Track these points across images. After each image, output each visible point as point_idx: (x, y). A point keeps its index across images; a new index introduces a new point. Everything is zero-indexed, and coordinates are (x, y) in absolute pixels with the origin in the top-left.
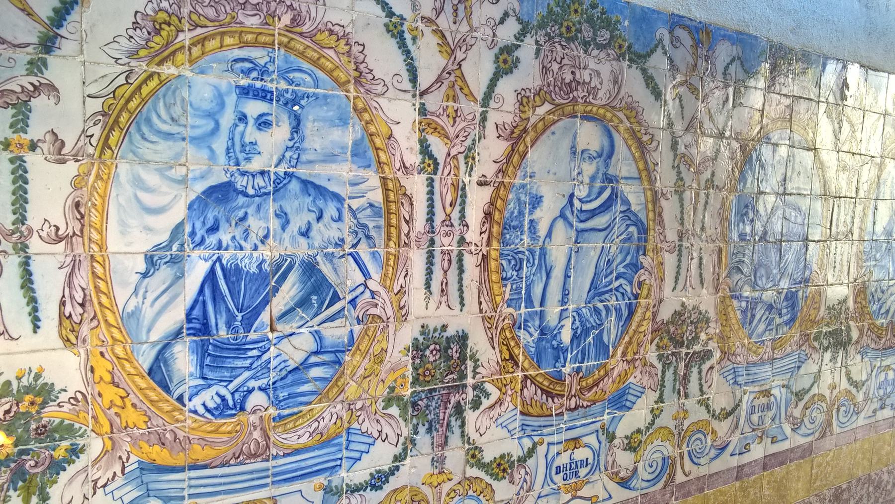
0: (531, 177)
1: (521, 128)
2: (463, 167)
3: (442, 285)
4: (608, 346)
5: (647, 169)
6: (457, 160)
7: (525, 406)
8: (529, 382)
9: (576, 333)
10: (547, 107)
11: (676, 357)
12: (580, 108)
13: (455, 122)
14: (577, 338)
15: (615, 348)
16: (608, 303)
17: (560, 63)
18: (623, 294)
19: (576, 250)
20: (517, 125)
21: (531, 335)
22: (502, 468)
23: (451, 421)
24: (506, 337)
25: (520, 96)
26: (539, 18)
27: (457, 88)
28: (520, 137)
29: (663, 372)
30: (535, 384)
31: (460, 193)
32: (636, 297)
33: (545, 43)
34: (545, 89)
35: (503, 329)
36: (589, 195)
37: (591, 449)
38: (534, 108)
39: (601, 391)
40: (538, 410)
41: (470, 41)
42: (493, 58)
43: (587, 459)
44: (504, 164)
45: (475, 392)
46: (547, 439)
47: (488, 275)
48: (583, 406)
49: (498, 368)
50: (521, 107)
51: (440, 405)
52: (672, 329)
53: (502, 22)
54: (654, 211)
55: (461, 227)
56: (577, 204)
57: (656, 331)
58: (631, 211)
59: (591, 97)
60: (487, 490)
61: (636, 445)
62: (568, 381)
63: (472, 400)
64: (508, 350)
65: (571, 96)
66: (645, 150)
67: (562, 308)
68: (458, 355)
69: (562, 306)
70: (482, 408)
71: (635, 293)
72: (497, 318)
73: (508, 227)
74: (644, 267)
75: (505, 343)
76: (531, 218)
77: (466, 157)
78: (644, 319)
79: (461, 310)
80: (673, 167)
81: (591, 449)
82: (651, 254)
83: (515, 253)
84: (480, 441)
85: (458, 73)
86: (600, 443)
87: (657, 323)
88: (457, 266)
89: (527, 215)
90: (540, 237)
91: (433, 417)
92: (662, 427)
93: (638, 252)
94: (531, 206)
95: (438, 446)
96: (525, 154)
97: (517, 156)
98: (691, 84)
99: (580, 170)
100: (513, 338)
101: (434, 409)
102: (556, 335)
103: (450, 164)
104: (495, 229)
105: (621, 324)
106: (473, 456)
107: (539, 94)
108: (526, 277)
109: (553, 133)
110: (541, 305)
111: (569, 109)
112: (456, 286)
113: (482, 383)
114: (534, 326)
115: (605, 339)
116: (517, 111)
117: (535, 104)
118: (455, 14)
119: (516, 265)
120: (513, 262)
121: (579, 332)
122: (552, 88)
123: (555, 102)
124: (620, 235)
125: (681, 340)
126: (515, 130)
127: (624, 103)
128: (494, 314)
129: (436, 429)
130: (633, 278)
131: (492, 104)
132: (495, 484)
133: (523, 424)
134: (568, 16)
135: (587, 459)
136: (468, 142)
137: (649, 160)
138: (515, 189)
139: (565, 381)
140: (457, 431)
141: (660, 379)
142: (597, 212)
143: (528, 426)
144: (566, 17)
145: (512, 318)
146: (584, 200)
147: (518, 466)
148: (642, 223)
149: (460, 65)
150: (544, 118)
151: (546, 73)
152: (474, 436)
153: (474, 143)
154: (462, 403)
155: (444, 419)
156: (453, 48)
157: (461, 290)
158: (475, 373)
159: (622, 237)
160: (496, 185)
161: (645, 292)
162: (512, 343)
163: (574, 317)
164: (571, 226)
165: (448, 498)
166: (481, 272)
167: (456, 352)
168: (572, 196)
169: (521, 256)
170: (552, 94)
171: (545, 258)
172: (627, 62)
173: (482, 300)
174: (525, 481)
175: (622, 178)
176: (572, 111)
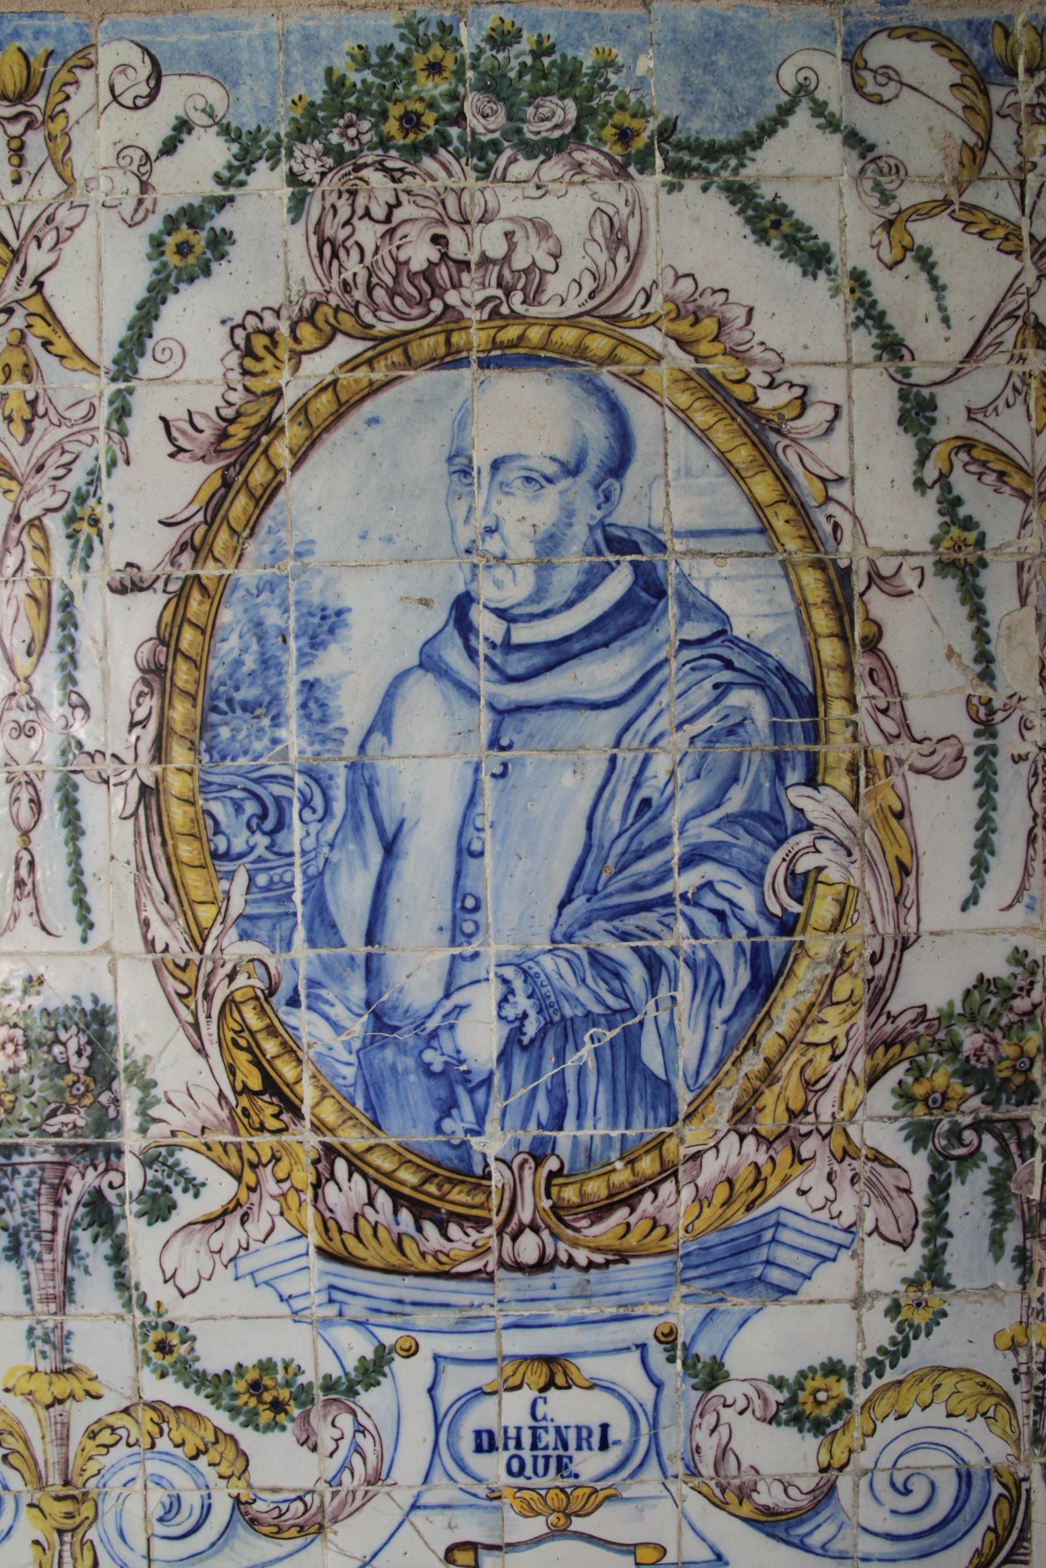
0: (299, 555)
1: (254, 420)
2: (60, 548)
3: (17, 868)
4: (668, 1084)
5: (790, 496)
6: (42, 529)
7: (334, 1232)
8: (341, 1167)
9: (520, 1030)
10: (343, 349)
11: (998, 1136)
12: (477, 338)
13: (29, 431)
14: (525, 1048)
15: (703, 1095)
16: (654, 943)
17: (388, 219)
18: (720, 915)
19: (498, 770)
20: (239, 414)
21: (337, 1027)
22: (268, 1397)
23: (76, 1240)
24: (245, 1027)
25: (240, 336)
26: (297, 113)
27: (34, 344)
28: (250, 446)
29: (939, 1187)
30: (365, 1176)
31: (56, 616)
32: (786, 925)
33: (323, 175)
34: (333, 300)
35: (230, 1001)
36: (538, 594)
37: (621, 1397)
38: (297, 356)
39: (647, 1225)
40: (384, 1252)
41: (65, 217)
42: (145, 247)
43: (605, 1427)
44: (196, 527)
45: (150, 1174)
46: (429, 1344)
47: (164, 843)
48: (571, 1263)
49: (224, 1114)
50: (249, 363)
51: (38, 1193)
52: (970, 1040)
53: (169, 147)
54: (844, 637)
55: (67, 710)
56: (487, 625)
57: (888, 1045)
58: (735, 641)
59: (517, 297)
60: (220, 1447)
61: (826, 1412)
62: (499, 1176)
63: (142, 1192)
64: (257, 1063)
65: (437, 306)
66: (774, 438)
67: (456, 951)
68: (85, 1063)
69: (453, 942)
70: (177, 1219)
71: (776, 910)
72: (208, 967)
73: (223, 705)
74: (810, 826)
75: (243, 1043)
76: (310, 675)
77: (72, 519)
78: (828, 1000)
79: (84, 940)
80: (919, 484)
81: (621, 1397)
82: (844, 783)
83: (257, 781)
84: (179, 1311)
85: (35, 305)
86: (659, 1385)
87: (892, 1018)
88: (59, 817)
89: (292, 667)
90: (344, 731)
91: (20, 1219)
92: (945, 1370)
93: (779, 774)
94: (305, 641)
95: (47, 1299)
96: (273, 490)
97: (242, 500)
98: (972, 208)
99: (490, 522)
100: (271, 1031)
101: (22, 1200)
102: (434, 1035)
103: (19, 542)
104: (180, 712)
105: (720, 1014)
106: (163, 1347)
107: (310, 319)
108: (304, 853)
109: (373, 421)
110: (370, 938)
111: (431, 345)
112: (65, 872)
113: (172, 1149)
114: (345, 1001)
115: (652, 1056)
116: (235, 376)
117: (299, 348)
118: (15, 161)
119: (263, 817)
120: (251, 808)
121: (531, 1028)
122: (359, 294)
123: (374, 332)
124: (689, 720)
125: (1019, 1080)
126: (232, 429)
127: (657, 298)
128: (195, 956)
129: (32, 1253)
130: (766, 861)
131: (146, 367)
132: (247, 1438)
133: (332, 1287)
134: (408, 86)
135: (605, 1427)
136: (76, 479)
137: (797, 471)
138: (240, 593)
139: (488, 1176)
140: (103, 1273)
141: (922, 1206)
142: (577, 647)
143: (354, 1294)
144: (400, 91)
145: (261, 970)
146: (516, 611)
147: (327, 1403)
148: (788, 679)
149: (38, 284)
150: (335, 382)
151: (335, 255)
152: (156, 1291)
153: (94, 478)
154: (111, 1195)
155: (54, 1231)
156: (15, 244)
157: (77, 881)
158: (148, 1120)
159: (701, 725)
160: (174, 587)
161: (824, 909)
162: (271, 1047)
163: (505, 981)
164: (473, 695)
165: (90, 1444)
166: (137, 833)
167: (79, 1053)
168: (462, 605)
169: (277, 789)
170: (363, 310)
171: (371, 795)
172: (659, 177)
173: (150, 913)
174: (358, 1450)
175: (677, 534)
176: (442, 350)
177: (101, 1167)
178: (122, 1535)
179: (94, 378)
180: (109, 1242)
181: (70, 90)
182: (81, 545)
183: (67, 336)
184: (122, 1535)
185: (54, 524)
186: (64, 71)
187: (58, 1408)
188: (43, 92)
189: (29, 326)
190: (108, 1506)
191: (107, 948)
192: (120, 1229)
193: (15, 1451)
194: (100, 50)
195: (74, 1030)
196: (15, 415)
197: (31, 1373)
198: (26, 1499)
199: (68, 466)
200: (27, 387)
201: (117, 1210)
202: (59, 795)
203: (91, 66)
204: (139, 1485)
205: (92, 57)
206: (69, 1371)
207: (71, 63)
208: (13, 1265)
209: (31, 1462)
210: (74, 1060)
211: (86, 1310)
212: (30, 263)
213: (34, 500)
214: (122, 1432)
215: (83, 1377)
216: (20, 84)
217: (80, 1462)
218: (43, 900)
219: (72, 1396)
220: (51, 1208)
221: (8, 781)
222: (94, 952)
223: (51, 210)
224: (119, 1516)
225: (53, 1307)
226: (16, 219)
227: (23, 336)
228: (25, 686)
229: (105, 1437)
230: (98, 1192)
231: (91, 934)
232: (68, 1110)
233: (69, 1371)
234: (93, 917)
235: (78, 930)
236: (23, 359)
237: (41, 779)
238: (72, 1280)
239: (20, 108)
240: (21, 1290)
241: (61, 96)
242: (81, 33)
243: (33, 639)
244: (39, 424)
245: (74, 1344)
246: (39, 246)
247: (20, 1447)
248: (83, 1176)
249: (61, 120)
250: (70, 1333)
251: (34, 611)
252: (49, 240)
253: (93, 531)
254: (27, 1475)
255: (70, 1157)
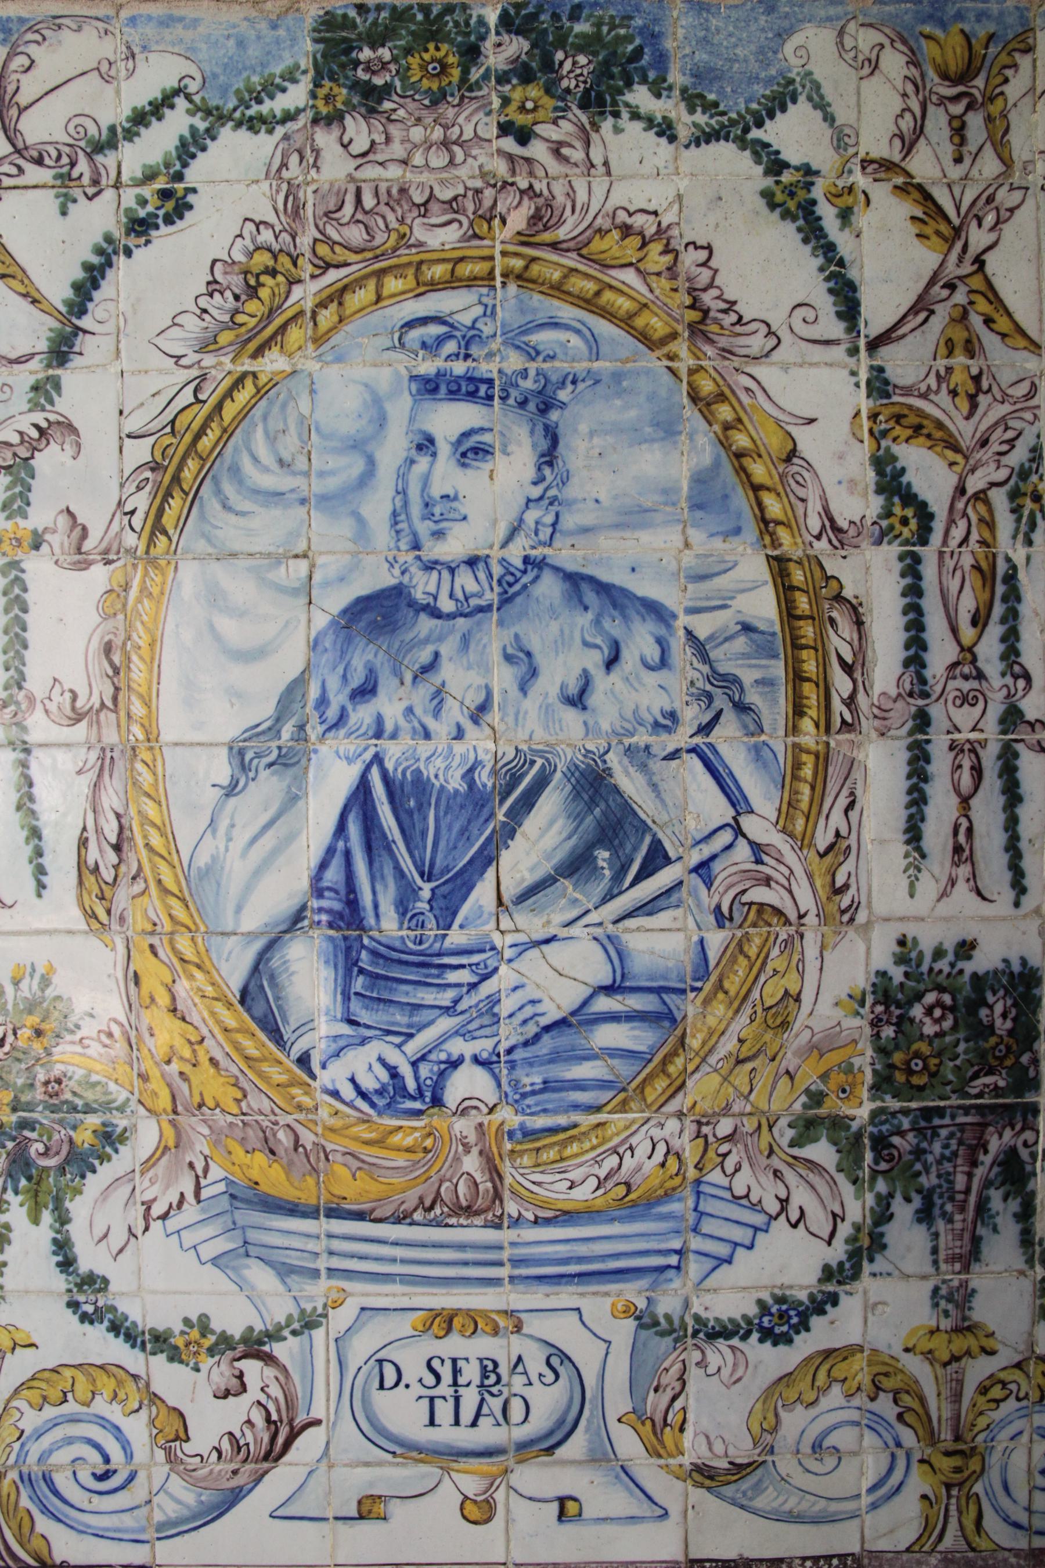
2: (1005, 523)
6: (987, 502)
13: (974, 406)
23: (988, 1199)
27: (976, 321)
31: (1000, 589)
41: (1005, 198)
55: (1009, 680)
68: (1009, 1024)
77: (1015, 495)
79: (1017, 904)
85: (976, 282)
88: (998, 784)
91: (934, 1180)
95: (952, 1259)
101: (939, 1162)
103: (964, 514)
118: (956, 140)
129: (944, 1214)
136: (1019, 456)
140: (1010, 1229)
149: (980, 262)
154: (1024, 1154)
155: (967, 1191)
156: (956, 221)
157: (1013, 848)
165: (981, 1400)
167: (1004, 1016)
177: (1018, 1127)
178: (1006, 1488)
179: (1035, 358)
180: (1019, 1200)
181: (1009, 73)
182: (1024, 520)
183: (1009, 315)
184: (1006, 1488)
185: (999, 498)
186: (1004, 55)
187: (955, 1365)
188: (983, 75)
189: (971, 303)
190: (995, 1460)
191: (1037, 911)
192: (1030, 1186)
193: (910, 1409)
194: (1039, 34)
195: (1001, 993)
196: (959, 389)
197: (932, 1333)
198: (917, 1456)
199: (1011, 443)
200: (970, 362)
201: (1028, 1168)
202: (1000, 763)
203: (1029, 50)
204: (1025, 1438)
205: (1030, 41)
206: (969, 1329)
207: (1011, 47)
208: (923, 1227)
209: (925, 1418)
210: (998, 1022)
211: (992, 1268)
212: (971, 240)
213: (979, 473)
214: (1013, 1387)
215: (981, 1334)
216: (962, 65)
217: (971, 1417)
218: (981, 866)
219: (968, 1353)
220: (966, 1169)
221: (951, 748)
222: (1025, 916)
223: (991, 190)
224: (1004, 1469)
225: (957, 1266)
226: (957, 196)
227: (965, 315)
228: (968, 656)
229: (996, 1392)
230: (1013, 1151)
231: (1024, 899)
232: (990, 1072)
233: (969, 1329)
234: (1026, 882)
235: (1010, 895)
236: (966, 334)
237: (983, 747)
238: (981, 1238)
239: (961, 89)
240: (928, 1250)
241: (999, 79)
242: (1022, 17)
243: (977, 610)
244: (983, 400)
245: (977, 1302)
246: (980, 225)
247: (915, 1405)
248: (1001, 1136)
249: (1000, 102)
250: (974, 1291)
251: (979, 583)
252: (990, 219)
253: (1036, 507)
254: (921, 1432)
255: (990, 1118)
